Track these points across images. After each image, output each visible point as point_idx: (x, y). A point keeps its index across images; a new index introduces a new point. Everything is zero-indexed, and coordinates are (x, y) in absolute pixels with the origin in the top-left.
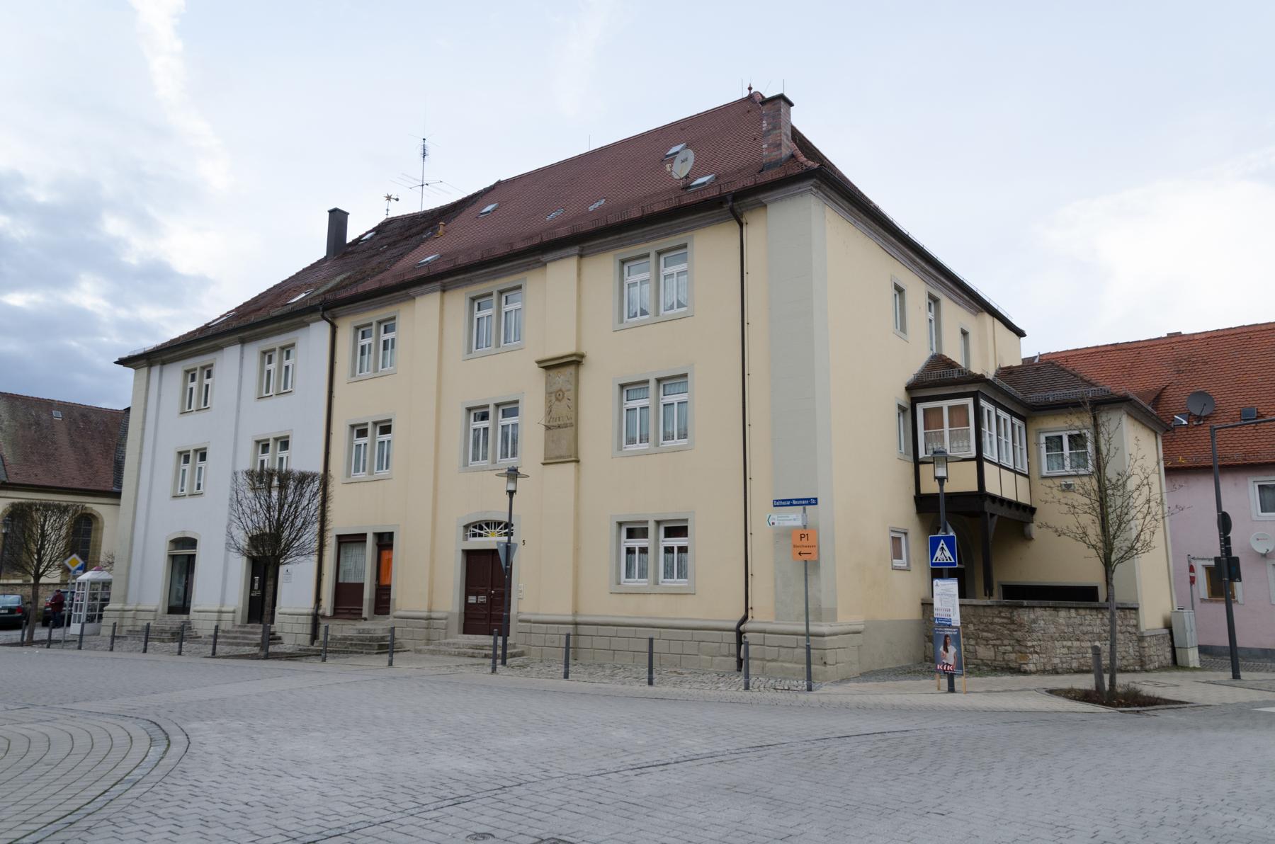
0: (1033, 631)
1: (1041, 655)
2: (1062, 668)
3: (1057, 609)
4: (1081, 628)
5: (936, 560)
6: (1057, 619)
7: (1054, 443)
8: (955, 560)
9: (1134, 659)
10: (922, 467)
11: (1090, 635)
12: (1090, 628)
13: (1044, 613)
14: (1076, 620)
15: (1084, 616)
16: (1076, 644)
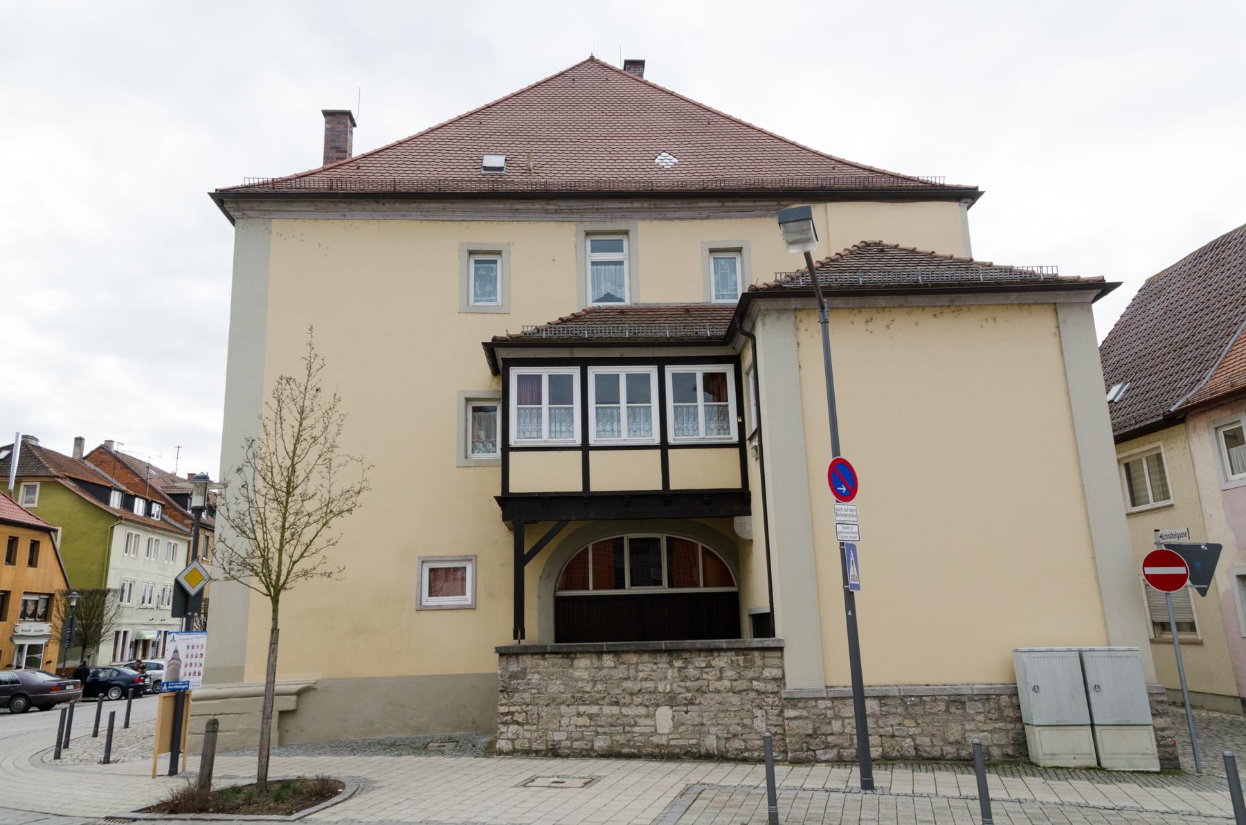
0: (515, 690)
1: (526, 727)
6: (571, 671)
7: (685, 389)
11: (647, 696)
13: (541, 662)
14: (613, 672)
15: (637, 664)
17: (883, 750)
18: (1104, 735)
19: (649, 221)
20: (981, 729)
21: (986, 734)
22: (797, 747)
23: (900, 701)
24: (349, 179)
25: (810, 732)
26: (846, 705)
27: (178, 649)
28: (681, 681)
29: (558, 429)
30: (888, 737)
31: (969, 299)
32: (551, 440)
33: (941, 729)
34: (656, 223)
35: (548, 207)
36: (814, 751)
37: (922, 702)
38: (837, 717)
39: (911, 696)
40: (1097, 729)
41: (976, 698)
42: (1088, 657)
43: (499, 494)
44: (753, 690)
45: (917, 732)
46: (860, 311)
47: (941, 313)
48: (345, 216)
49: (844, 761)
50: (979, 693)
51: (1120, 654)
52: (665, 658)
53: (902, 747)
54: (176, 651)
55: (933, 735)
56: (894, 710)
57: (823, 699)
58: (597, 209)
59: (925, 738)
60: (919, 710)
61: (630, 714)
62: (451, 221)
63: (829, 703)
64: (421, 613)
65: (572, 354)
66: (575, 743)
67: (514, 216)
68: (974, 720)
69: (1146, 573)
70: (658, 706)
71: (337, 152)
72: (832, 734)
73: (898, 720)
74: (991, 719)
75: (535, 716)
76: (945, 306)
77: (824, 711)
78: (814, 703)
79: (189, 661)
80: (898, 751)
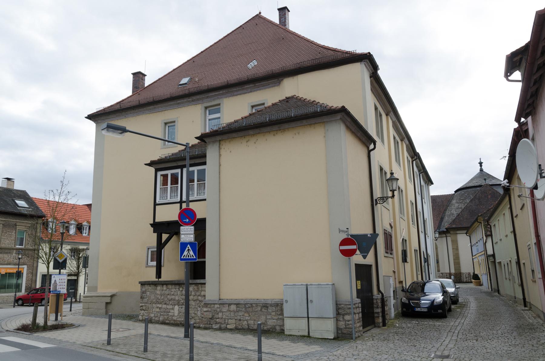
2: (154, 320)
3: (157, 285)
4: (169, 297)
5: (184, 257)
8: (196, 257)
9: (199, 319)
10: (157, 206)
12: (173, 297)
14: (166, 292)
16: (164, 306)
17: (236, 326)
18: (313, 322)
19: (228, 98)
20: (273, 318)
21: (275, 320)
22: (206, 323)
23: (244, 306)
24: (144, 97)
25: (211, 317)
26: (224, 306)
27: (56, 280)
28: (181, 296)
29: (174, 195)
30: (238, 320)
31: (286, 126)
32: (171, 200)
33: (258, 317)
34: (231, 98)
35: (189, 100)
36: (212, 324)
37: (252, 306)
38: (221, 311)
39: (248, 304)
40: (310, 319)
41: (273, 305)
42: (309, 287)
43: (152, 223)
44: (198, 300)
45: (249, 319)
46: (245, 137)
47: (277, 133)
48: (126, 117)
49: (222, 329)
50: (274, 303)
51: (323, 286)
52: (177, 287)
53: (242, 324)
54: (55, 281)
55: (255, 320)
56: (241, 309)
57: (216, 304)
58: (207, 97)
59: (251, 321)
60: (250, 309)
61: (169, 308)
62: (159, 112)
63: (218, 306)
64: (147, 268)
65: (177, 164)
66: (156, 318)
67: (179, 106)
68: (271, 314)
69: (340, 249)
70: (175, 305)
71: (136, 89)
72: (218, 318)
73: (242, 313)
74: (278, 314)
75: (148, 307)
76: (278, 130)
77: (216, 309)
78: (213, 306)
79: (60, 284)
80: (241, 326)
